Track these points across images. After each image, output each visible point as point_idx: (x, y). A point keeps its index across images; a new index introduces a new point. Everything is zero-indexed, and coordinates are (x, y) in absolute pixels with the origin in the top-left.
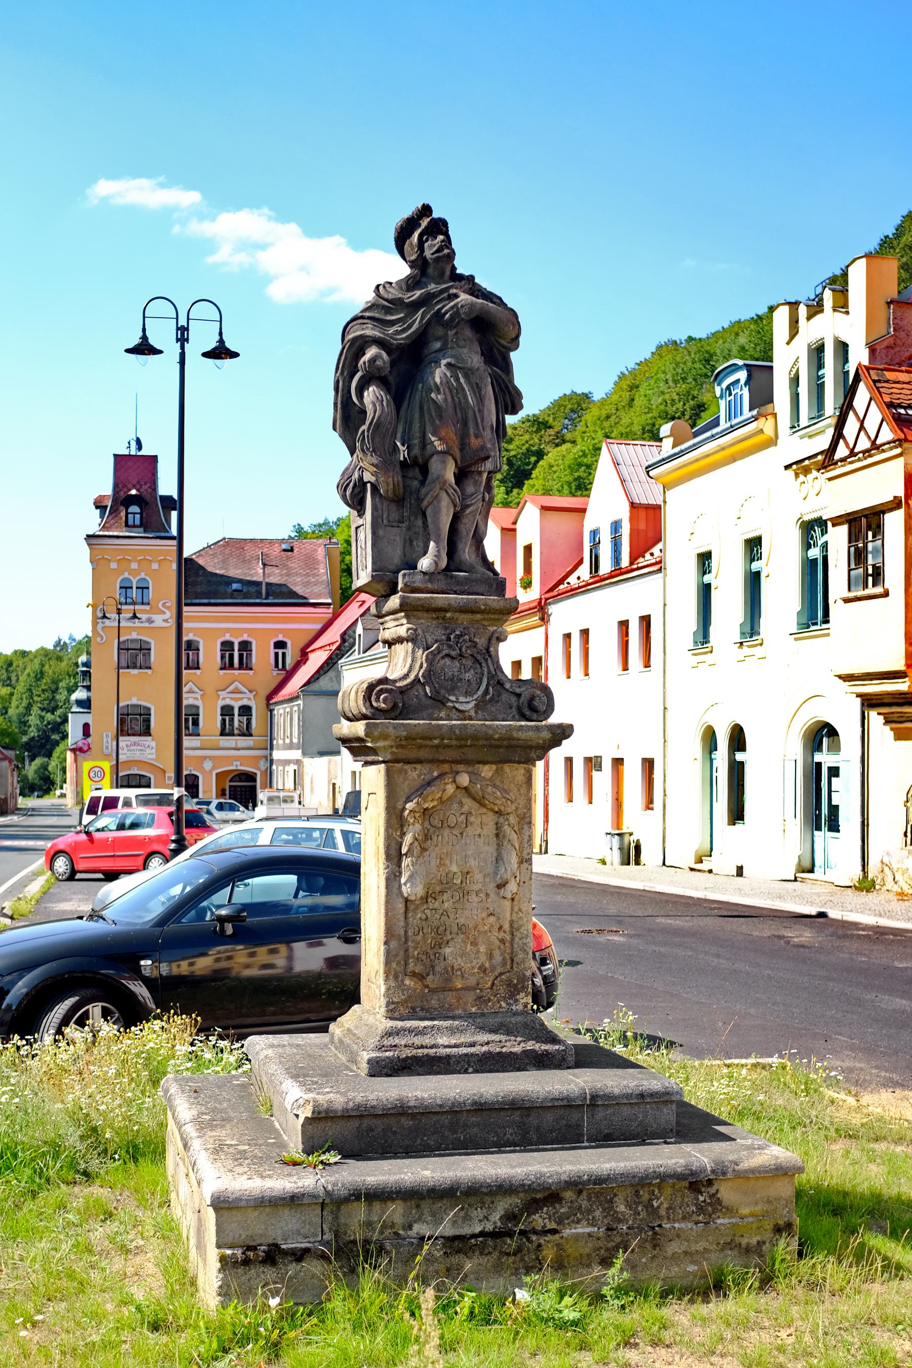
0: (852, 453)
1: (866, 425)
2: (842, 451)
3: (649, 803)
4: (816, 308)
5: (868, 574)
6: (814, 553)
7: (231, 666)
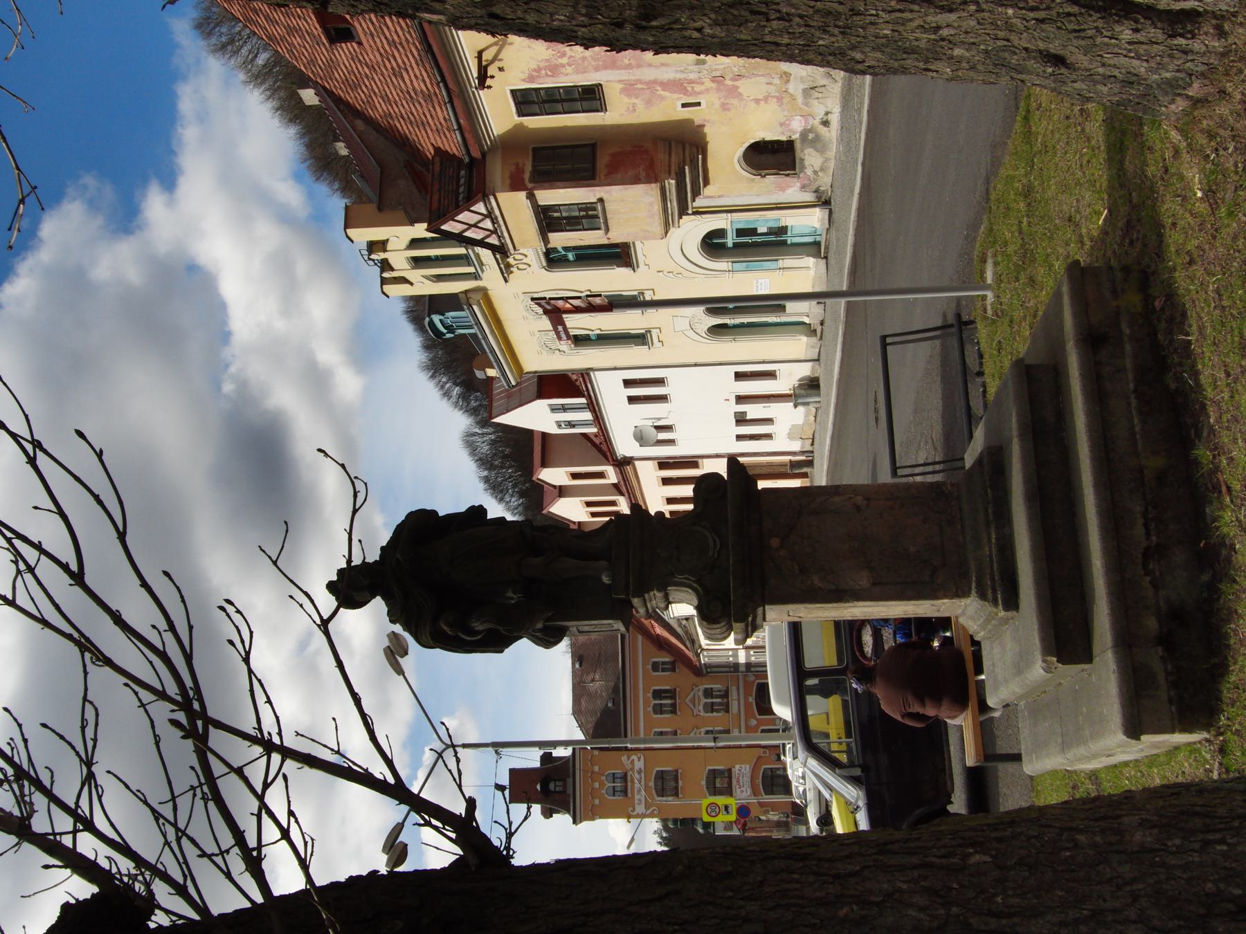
0: (494, 232)
1: (472, 222)
2: (493, 240)
3: (771, 375)
4: (385, 265)
5: (587, 217)
6: (571, 256)
7: (674, 705)
